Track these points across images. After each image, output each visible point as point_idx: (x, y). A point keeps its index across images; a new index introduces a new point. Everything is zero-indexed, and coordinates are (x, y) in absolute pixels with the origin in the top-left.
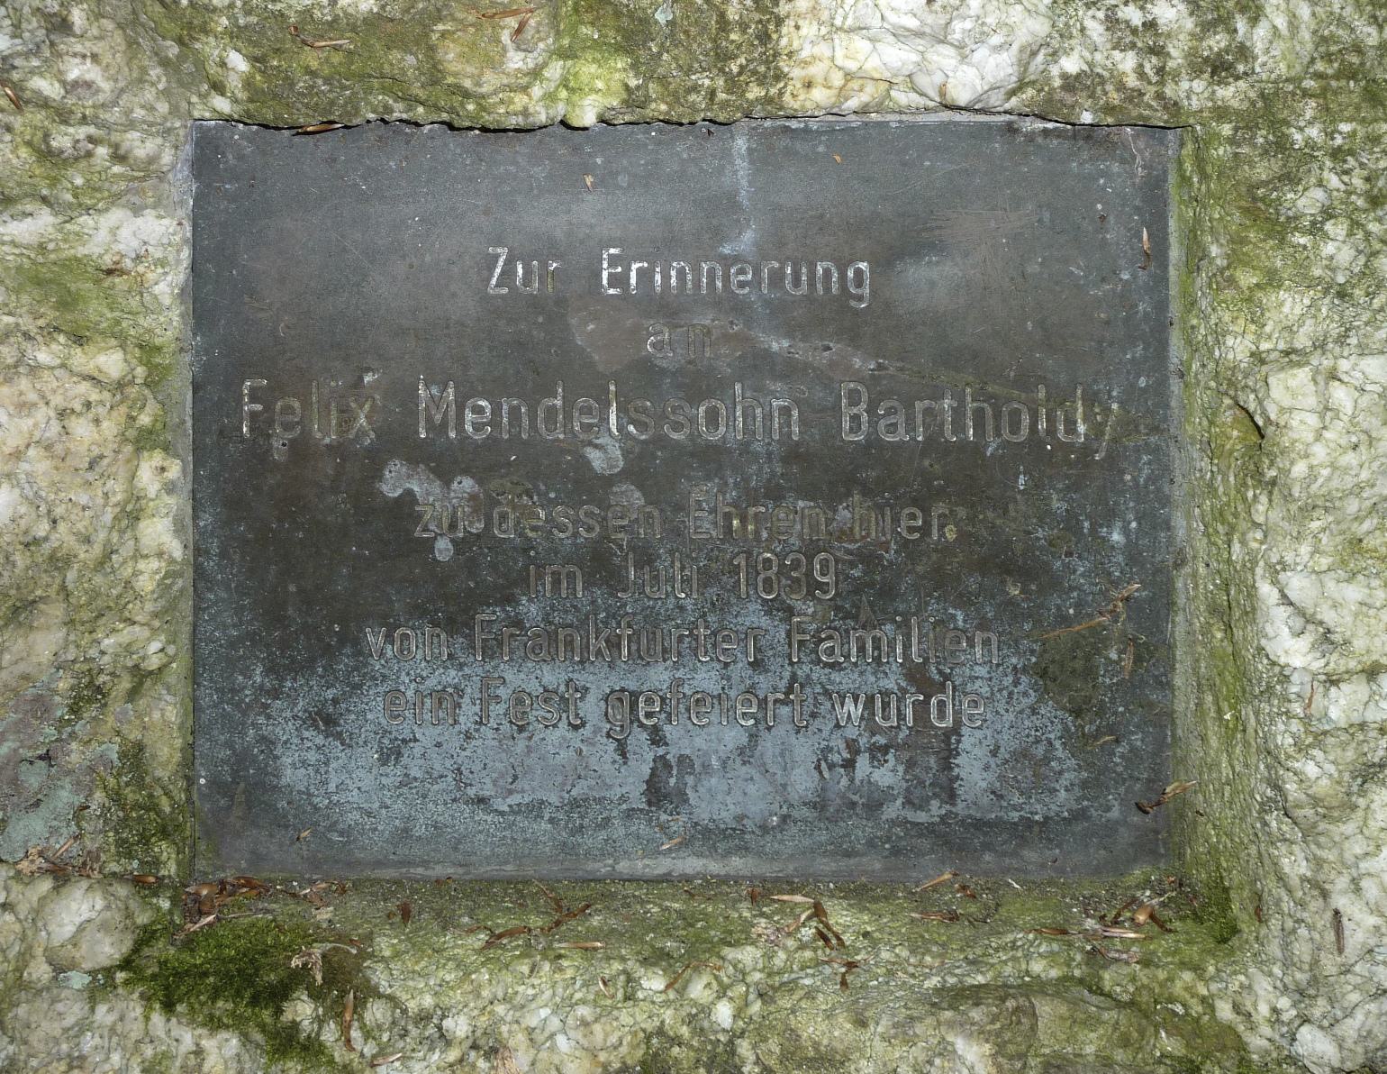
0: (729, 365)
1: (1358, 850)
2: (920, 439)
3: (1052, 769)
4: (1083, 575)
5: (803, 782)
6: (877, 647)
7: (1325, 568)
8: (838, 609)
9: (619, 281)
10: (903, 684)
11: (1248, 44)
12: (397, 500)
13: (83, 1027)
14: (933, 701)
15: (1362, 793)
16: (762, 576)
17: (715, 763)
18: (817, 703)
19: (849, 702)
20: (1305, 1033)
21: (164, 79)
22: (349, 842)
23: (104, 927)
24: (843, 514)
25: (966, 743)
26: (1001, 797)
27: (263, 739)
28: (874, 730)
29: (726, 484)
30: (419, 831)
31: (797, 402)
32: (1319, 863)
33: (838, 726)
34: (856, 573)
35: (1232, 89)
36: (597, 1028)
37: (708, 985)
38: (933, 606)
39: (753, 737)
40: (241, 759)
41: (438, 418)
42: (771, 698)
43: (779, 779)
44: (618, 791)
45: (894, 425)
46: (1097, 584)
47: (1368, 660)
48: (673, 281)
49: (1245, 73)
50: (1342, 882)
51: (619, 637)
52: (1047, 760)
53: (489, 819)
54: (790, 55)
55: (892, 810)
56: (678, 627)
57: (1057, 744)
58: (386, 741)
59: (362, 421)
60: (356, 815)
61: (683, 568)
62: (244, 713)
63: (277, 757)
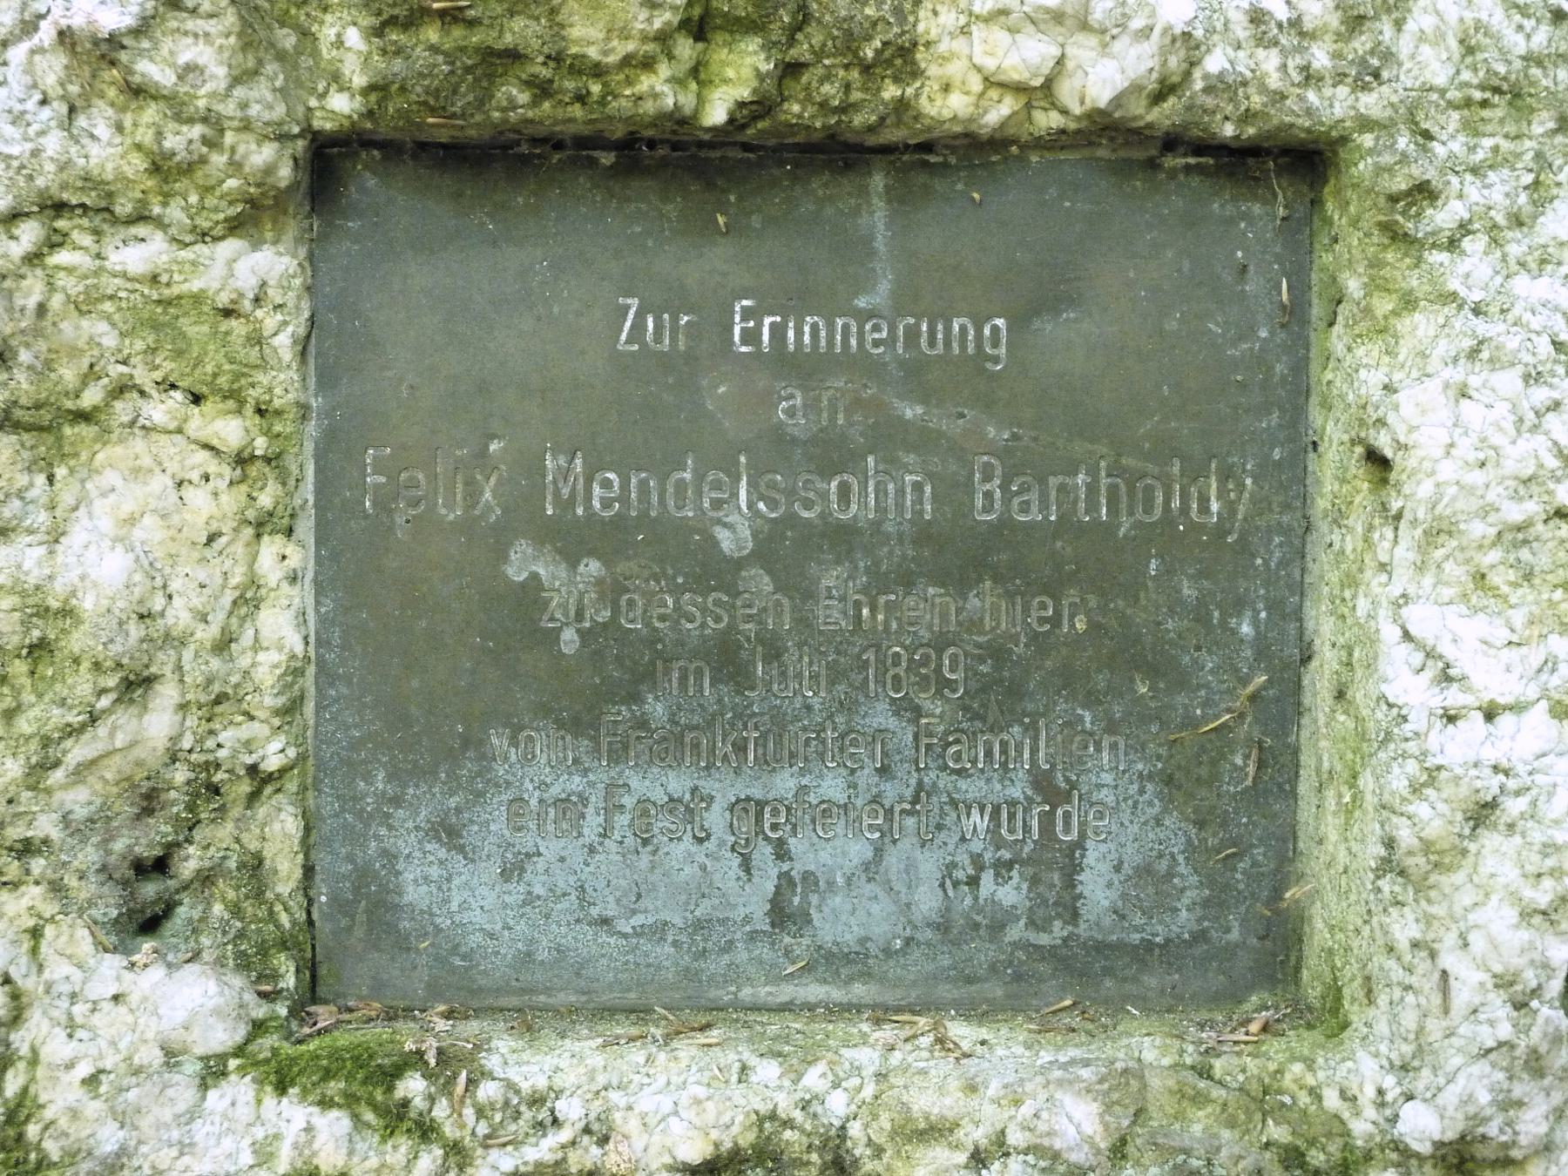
0: (861, 434)
1: (1467, 901)
2: (1053, 518)
3: (1174, 887)
4: (1211, 671)
5: (927, 901)
6: (1004, 751)
7: (1446, 600)
8: (966, 709)
9: (751, 337)
10: (1029, 793)
11: (1394, 50)
12: (523, 585)
13: (192, 1115)
14: (1060, 812)
15: (1473, 836)
16: (891, 672)
17: (840, 880)
18: (943, 814)
19: (975, 812)
20: (1408, 1111)
21: (281, 77)
22: (471, 967)
23: (217, 1012)
24: (973, 602)
25: (1091, 857)
26: (1123, 917)
27: (385, 853)
28: (999, 844)
29: (856, 567)
30: (543, 955)
31: (930, 476)
32: (1428, 920)
33: (963, 839)
34: (984, 668)
35: (1375, 95)
36: (710, 1105)
37: (824, 1075)
38: (1061, 706)
39: (879, 851)
40: (363, 875)
41: (566, 492)
42: (897, 809)
43: (904, 898)
44: (742, 912)
45: (1027, 503)
46: (1224, 682)
47: (1486, 697)
48: (807, 339)
49: (1390, 81)
50: (1450, 939)
51: (746, 739)
52: (1170, 875)
53: (612, 941)
54: (928, 44)
55: (1015, 932)
56: (805, 729)
57: (1181, 858)
58: (509, 855)
59: (488, 495)
60: (477, 938)
61: (811, 663)
62: (367, 826)
63: (399, 873)
